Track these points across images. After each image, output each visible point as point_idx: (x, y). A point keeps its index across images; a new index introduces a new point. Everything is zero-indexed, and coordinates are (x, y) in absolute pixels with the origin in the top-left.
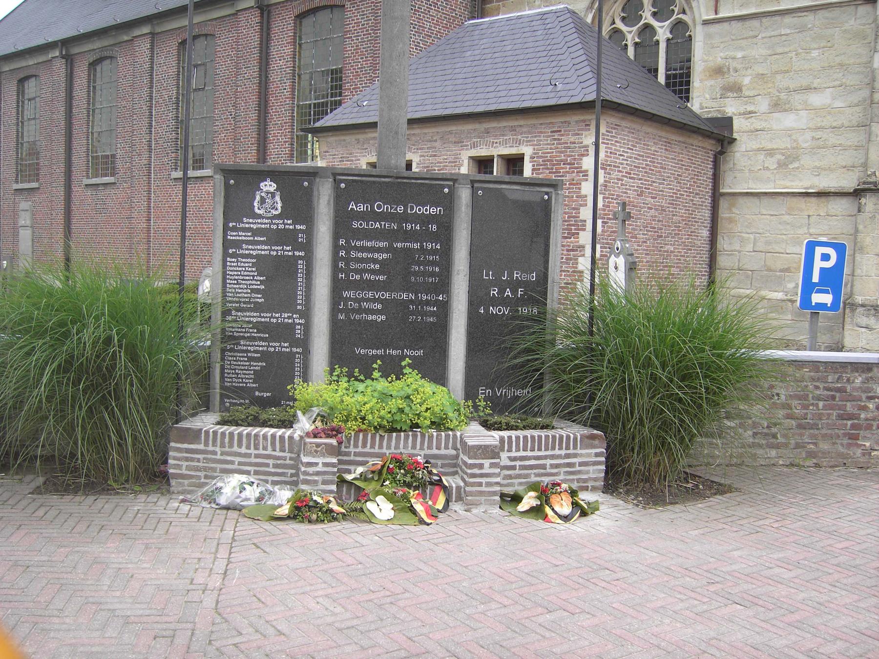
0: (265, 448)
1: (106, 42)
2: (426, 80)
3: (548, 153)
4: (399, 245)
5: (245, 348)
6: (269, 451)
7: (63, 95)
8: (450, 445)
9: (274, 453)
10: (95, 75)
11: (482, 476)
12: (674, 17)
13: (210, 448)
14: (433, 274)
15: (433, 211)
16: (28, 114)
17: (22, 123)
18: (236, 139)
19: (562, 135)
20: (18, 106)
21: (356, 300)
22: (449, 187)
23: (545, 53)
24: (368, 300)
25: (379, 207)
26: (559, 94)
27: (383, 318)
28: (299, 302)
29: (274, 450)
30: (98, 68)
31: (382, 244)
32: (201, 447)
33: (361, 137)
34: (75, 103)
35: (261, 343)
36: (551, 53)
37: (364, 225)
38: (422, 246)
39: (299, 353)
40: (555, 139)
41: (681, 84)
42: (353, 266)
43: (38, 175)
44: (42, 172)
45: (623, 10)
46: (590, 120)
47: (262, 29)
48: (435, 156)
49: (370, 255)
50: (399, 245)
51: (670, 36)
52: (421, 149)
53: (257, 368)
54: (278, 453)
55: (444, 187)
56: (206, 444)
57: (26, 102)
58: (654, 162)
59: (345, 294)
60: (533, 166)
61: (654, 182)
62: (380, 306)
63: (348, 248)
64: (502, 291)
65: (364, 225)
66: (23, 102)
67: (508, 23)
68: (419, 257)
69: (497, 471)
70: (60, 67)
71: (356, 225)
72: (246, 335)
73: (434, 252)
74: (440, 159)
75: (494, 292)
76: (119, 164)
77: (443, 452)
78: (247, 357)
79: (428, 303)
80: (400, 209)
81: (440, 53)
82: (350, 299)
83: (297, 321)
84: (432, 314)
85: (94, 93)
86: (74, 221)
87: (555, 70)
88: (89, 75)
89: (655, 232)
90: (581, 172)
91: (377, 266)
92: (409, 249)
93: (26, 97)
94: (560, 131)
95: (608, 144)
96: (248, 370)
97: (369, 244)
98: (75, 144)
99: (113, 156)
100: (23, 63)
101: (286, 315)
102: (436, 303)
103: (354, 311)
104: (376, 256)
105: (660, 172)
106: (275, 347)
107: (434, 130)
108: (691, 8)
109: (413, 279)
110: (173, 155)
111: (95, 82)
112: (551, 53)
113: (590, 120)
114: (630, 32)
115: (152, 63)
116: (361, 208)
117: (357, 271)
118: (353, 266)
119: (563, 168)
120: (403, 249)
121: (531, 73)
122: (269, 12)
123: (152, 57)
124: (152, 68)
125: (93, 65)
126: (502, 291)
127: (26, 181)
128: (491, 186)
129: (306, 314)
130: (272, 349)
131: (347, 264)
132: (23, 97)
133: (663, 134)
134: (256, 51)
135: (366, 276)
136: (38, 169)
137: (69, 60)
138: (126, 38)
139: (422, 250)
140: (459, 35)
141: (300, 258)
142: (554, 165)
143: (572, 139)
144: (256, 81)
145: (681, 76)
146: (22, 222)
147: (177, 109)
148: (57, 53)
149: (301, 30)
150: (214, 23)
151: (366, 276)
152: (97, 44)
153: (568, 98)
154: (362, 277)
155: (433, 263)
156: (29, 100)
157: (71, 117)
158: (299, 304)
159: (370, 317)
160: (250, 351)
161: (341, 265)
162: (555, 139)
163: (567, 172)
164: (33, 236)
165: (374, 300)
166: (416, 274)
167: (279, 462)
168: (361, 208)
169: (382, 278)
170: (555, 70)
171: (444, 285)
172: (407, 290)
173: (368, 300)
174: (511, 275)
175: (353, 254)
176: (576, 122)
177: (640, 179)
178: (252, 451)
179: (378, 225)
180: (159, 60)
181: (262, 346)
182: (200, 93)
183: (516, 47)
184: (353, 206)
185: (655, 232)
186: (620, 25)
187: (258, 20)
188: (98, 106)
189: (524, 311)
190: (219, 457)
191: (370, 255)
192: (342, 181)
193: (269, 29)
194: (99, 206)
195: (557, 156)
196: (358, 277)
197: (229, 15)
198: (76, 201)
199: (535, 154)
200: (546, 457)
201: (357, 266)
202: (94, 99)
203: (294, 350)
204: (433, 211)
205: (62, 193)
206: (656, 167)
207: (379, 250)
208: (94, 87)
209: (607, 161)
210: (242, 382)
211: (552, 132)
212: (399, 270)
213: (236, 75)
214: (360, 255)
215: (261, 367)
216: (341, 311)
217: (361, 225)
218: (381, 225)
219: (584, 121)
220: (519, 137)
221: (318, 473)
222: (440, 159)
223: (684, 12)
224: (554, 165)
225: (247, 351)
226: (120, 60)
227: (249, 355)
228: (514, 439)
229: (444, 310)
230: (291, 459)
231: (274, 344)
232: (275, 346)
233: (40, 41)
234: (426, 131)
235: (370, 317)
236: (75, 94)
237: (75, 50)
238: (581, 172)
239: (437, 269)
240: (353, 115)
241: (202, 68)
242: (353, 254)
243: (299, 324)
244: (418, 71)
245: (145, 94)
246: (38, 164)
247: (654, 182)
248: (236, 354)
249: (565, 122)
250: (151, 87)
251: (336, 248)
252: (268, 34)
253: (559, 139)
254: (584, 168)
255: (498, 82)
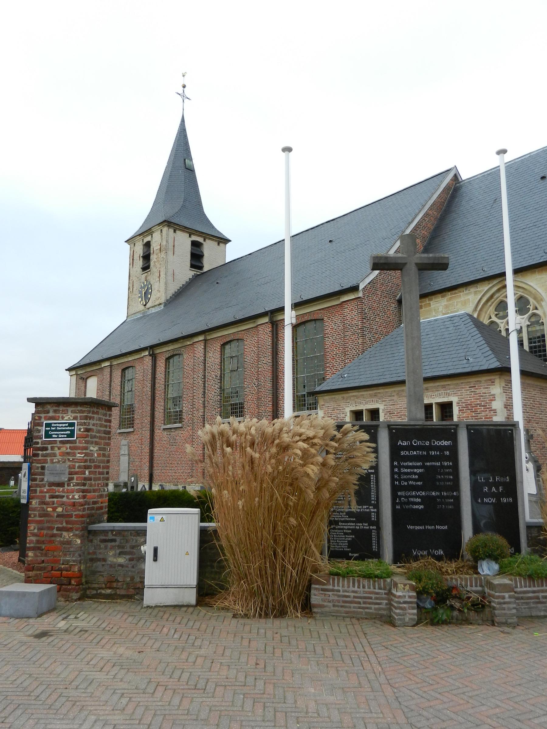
0: (369, 588)
1: (176, 346)
2: (382, 360)
3: (469, 400)
4: (428, 464)
5: (342, 527)
6: (372, 589)
7: (150, 377)
8: (478, 585)
9: (375, 590)
10: (169, 365)
11: (504, 603)
12: (530, 312)
13: (336, 588)
14: (449, 480)
15: (446, 443)
16: (126, 389)
17: (124, 394)
18: (259, 399)
19: (477, 389)
20: (121, 384)
21: (406, 497)
22: (454, 429)
23: (457, 341)
24: (413, 497)
25: (415, 443)
26: (472, 365)
27: (422, 507)
28: (373, 499)
29: (375, 588)
30: (171, 361)
31: (419, 464)
32: (331, 587)
33: (346, 395)
34: (157, 381)
35: (351, 524)
36: (461, 340)
37: (407, 453)
38: (441, 464)
39: (374, 529)
40: (472, 392)
41: (540, 351)
42: (403, 477)
43: (133, 424)
44: (136, 422)
45: (496, 310)
46: (494, 379)
47: (273, 335)
48: (394, 405)
49: (412, 470)
50: (428, 464)
51: (529, 323)
52: (384, 401)
53: (349, 539)
54: (377, 591)
55: (451, 429)
56: (334, 586)
57: (126, 382)
58: (534, 401)
59: (399, 493)
60: (459, 408)
61: (536, 414)
62: (419, 500)
63: (400, 467)
64: (490, 489)
65: (407, 453)
66: (124, 382)
67: (429, 324)
68: (441, 470)
69: (513, 600)
70: (148, 361)
71: (402, 453)
72: (342, 519)
73: (448, 467)
74: (398, 407)
75: (486, 489)
76: (184, 416)
77: (474, 588)
78: (343, 532)
79: (448, 497)
80: (427, 443)
81: (388, 344)
82: (402, 496)
83: (372, 510)
84: (450, 504)
85: (169, 375)
86: (156, 451)
87: (466, 350)
88: (166, 365)
89: (541, 444)
90: (491, 410)
91: (417, 477)
92: (434, 466)
93: (126, 379)
94: (475, 387)
95: (506, 393)
96: (344, 540)
97: (411, 464)
98: (157, 404)
99: (181, 411)
100: (126, 360)
101: (365, 507)
102: (452, 497)
103: (405, 503)
104: (416, 470)
105: (539, 407)
106: (359, 526)
107: (393, 389)
108: (541, 306)
109: (438, 483)
110: (219, 409)
111: (169, 369)
112: (461, 340)
113: (494, 379)
114: (502, 323)
115: (205, 357)
116: (405, 443)
117: (406, 480)
118: (403, 477)
119: (479, 409)
120: (431, 466)
121: (450, 353)
122: (277, 325)
123: (205, 353)
124: (205, 360)
125: (168, 359)
126: (490, 489)
127: (125, 428)
128: (478, 427)
129: (377, 506)
130: (358, 528)
131: (399, 476)
132: (125, 379)
133: (538, 384)
134: (270, 347)
135: (410, 483)
136: (133, 420)
137: (154, 357)
138: (189, 343)
139: (442, 467)
140: (399, 333)
141: (372, 473)
142: (473, 407)
143: (484, 391)
144: (270, 364)
145: (539, 346)
146: (122, 452)
147: (221, 382)
148: (147, 353)
149: (296, 334)
150: (243, 332)
151: (410, 483)
152: (171, 347)
153: (478, 367)
154: (408, 483)
155: (449, 474)
156: (128, 380)
157: (154, 389)
158: (373, 500)
159: (415, 507)
160: (345, 529)
161: (396, 476)
162: (472, 392)
163: (482, 411)
164: (129, 460)
165: (416, 497)
166: (440, 480)
167: (378, 596)
168: (405, 443)
169: (419, 483)
170: (466, 350)
171: (456, 486)
172: (435, 490)
173: (413, 497)
174: (494, 479)
175: (403, 470)
176: (485, 381)
177: (528, 412)
178: (351, 588)
179: (415, 453)
180: (210, 355)
181: (352, 526)
182: (235, 373)
183: (437, 338)
184: (400, 443)
185: (541, 444)
186: (494, 319)
187: (270, 329)
188: (171, 382)
189: (504, 500)
190: (341, 593)
191: (412, 470)
192: (394, 429)
193: (277, 334)
194: (171, 441)
195: (474, 402)
196: (406, 483)
197: (252, 328)
198: (157, 438)
199: (460, 401)
200: (538, 592)
201: (405, 477)
202: (168, 378)
203: (371, 527)
204: (446, 443)
205: (149, 434)
206: (536, 404)
207: (417, 467)
208: (169, 372)
209: (507, 403)
210: (341, 548)
211: (469, 387)
212: (429, 479)
213: (258, 361)
214: (406, 470)
215: (352, 538)
216: (398, 504)
217: (405, 453)
218: (417, 453)
219: (490, 380)
220: (448, 391)
221: (405, 602)
222: (398, 407)
223: (536, 309)
224: (473, 407)
225: (343, 529)
226: (185, 356)
227: (344, 531)
228: (372, 587)
229: (457, 500)
230: (385, 594)
231: (359, 524)
232: (360, 526)
233: (137, 347)
234: (387, 390)
235: (415, 507)
236: (157, 376)
237: (158, 351)
238: (491, 410)
239: (451, 477)
240: (339, 383)
241: (236, 358)
242: (403, 470)
243: (374, 512)
244: (376, 355)
245: (201, 375)
246: (133, 417)
247: (536, 414)
248: (336, 531)
249: (478, 381)
250: (205, 370)
251: (392, 467)
252: (277, 337)
253: (474, 392)
254: (494, 408)
255: (431, 359)
